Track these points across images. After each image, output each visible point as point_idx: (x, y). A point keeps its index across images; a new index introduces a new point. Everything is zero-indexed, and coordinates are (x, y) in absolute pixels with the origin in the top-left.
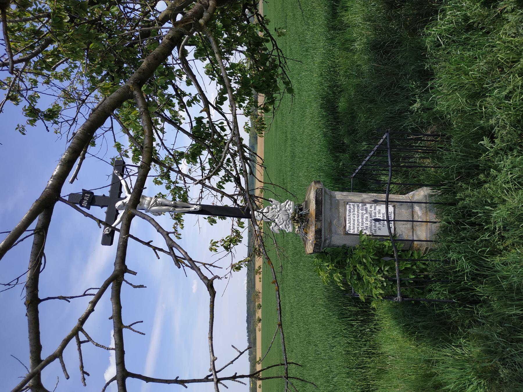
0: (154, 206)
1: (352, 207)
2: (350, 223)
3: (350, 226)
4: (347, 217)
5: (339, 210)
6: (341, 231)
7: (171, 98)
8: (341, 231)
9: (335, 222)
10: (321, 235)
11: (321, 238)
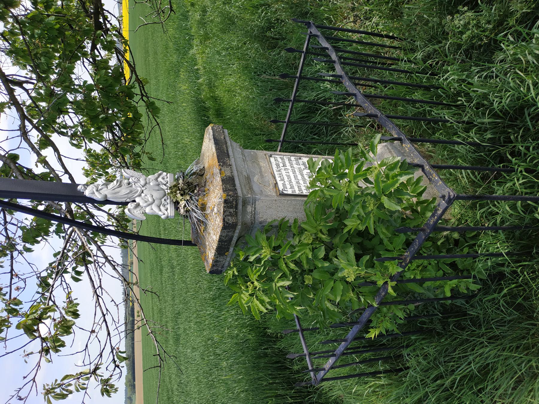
1: (280, 160)
2: (282, 180)
3: (284, 185)
4: (276, 173)
5: (258, 164)
6: (270, 191)
7: (59, 337)
8: (270, 191)
9: (256, 179)
10: (234, 185)
11: (236, 189)
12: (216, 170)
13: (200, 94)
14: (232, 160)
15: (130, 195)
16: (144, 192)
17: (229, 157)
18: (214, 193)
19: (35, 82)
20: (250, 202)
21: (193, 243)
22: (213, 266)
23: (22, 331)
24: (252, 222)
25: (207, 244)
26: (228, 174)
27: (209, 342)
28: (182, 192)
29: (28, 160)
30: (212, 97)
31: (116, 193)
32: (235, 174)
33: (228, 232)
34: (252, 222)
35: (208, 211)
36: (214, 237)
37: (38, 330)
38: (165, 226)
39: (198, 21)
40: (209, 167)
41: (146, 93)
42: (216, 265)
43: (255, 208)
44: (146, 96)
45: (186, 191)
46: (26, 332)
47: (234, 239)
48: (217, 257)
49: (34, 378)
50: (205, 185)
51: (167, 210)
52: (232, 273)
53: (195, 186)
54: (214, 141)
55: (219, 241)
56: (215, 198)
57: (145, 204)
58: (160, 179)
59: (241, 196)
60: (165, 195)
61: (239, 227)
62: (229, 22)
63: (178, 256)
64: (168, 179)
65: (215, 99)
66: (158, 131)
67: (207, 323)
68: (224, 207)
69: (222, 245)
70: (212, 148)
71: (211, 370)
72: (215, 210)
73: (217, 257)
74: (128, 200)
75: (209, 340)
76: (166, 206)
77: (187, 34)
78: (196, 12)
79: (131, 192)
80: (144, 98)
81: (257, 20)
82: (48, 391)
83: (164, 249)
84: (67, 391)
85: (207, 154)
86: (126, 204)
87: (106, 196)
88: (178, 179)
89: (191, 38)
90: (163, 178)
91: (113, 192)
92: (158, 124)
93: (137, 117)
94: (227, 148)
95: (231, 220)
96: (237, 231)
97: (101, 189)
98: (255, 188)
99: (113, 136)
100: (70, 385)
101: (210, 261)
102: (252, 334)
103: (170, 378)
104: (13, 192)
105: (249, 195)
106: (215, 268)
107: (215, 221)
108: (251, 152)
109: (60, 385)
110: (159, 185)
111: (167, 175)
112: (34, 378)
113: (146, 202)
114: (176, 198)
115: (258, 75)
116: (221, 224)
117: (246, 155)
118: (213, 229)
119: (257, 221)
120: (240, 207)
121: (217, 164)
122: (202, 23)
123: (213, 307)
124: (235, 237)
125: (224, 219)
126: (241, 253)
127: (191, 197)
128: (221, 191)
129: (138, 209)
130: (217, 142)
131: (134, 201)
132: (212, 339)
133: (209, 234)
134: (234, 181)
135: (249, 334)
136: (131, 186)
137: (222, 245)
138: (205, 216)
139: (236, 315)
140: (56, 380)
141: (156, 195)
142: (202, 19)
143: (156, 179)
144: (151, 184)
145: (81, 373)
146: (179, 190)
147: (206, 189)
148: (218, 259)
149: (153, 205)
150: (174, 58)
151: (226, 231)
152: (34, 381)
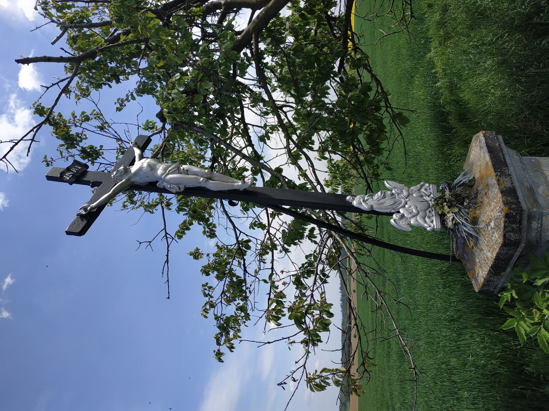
0: (173, 173)
5: (543, 173)
10: (517, 198)
11: (519, 202)
12: (493, 181)
13: (438, 99)
14: (511, 169)
15: (394, 206)
16: (408, 203)
17: (507, 167)
18: (490, 206)
19: (294, 105)
20: (535, 218)
21: (458, 258)
22: (484, 285)
23: (293, 321)
24: (537, 241)
25: (477, 260)
26: (508, 185)
27: (443, 366)
28: (449, 204)
29: (291, 173)
30: (454, 100)
31: (381, 204)
32: (517, 184)
33: (509, 250)
34: (537, 241)
35: (482, 225)
36: (489, 254)
37: (305, 322)
38: (389, 237)
39: (437, 22)
40: (482, 178)
41: (390, 104)
42: (488, 285)
43: (542, 225)
44: (390, 107)
45: (454, 203)
46: (296, 323)
47: (513, 258)
48: (491, 277)
49: (305, 364)
50: (476, 197)
51: (432, 222)
52: (510, 295)
53: (464, 198)
54: (488, 148)
55: (495, 259)
56: (492, 210)
57: (410, 216)
58: (423, 190)
59: (527, 210)
60: (429, 207)
61: (523, 245)
62: (478, 17)
63: (405, 269)
64: (431, 191)
65: (458, 102)
66: (401, 141)
67: (441, 345)
68: (505, 222)
69: (499, 263)
70: (484, 157)
71: (444, 397)
72: (492, 224)
73: (491, 277)
74: (393, 211)
75: (443, 364)
76: (431, 218)
77: (423, 38)
78: (435, 12)
79: (395, 203)
80: (389, 110)
81: (520, 8)
82: (310, 379)
83: (388, 261)
84: (325, 382)
85: (479, 164)
86: (391, 214)
87: (372, 206)
88: (443, 191)
89: (428, 41)
90: (426, 190)
91: (378, 202)
92: (401, 134)
93: (381, 129)
94: (504, 156)
95: (513, 237)
96: (520, 250)
97: (367, 200)
98: (541, 201)
99: (354, 149)
100: (328, 378)
101: (481, 280)
102: (503, 368)
103: (391, 394)
104: (295, 201)
105: (535, 209)
106: (486, 288)
107: (492, 236)
108: (531, 159)
109: (320, 377)
110: (422, 196)
111: (429, 186)
112: (305, 364)
113: (411, 213)
114: (442, 210)
115: (523, 70)
116: (501, 241)
117: (525, 163)
118: (487, 246)
119: (543, 240)
120: (525, 222)
121: (493, 174)
122: (442, 24)
123: (450, 329)
124: (515, 256)
125: (504, 236)
126: (524, 275)
127: (460, 210)
128: (501, 204)
129: (403, 220)
130: (491, 150)
131: (399, 212)
132: (447, 363)
133: (481, 250)
134: (516, 193)
135: (499, 367)
136: (395, 198)
137: (499, 263)
138: (478, 231)
139: (482, 342)
140: (316, 371)
141: (420, 206)
142: (442, 18)
143: (419, 190)
144: (414, 195)
145: (337, 369)
146: (446, 201)
147: (478, 201)
148: (492, 279)
149: (418, 218)
150: (408, 64)
151: (506, 248)
152: (305, 368)
